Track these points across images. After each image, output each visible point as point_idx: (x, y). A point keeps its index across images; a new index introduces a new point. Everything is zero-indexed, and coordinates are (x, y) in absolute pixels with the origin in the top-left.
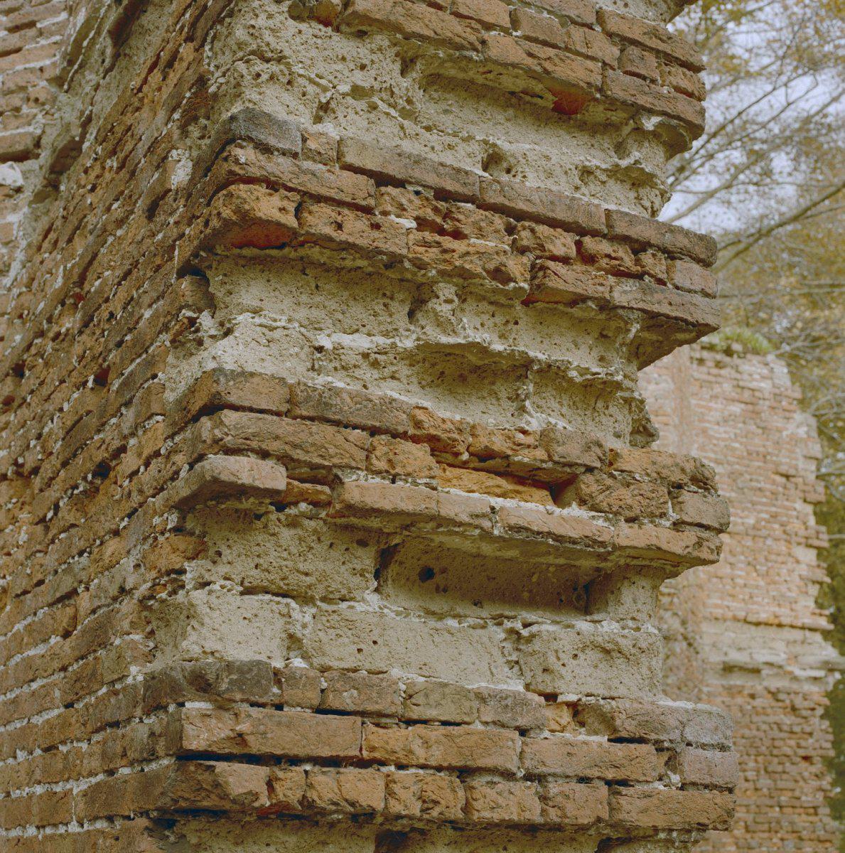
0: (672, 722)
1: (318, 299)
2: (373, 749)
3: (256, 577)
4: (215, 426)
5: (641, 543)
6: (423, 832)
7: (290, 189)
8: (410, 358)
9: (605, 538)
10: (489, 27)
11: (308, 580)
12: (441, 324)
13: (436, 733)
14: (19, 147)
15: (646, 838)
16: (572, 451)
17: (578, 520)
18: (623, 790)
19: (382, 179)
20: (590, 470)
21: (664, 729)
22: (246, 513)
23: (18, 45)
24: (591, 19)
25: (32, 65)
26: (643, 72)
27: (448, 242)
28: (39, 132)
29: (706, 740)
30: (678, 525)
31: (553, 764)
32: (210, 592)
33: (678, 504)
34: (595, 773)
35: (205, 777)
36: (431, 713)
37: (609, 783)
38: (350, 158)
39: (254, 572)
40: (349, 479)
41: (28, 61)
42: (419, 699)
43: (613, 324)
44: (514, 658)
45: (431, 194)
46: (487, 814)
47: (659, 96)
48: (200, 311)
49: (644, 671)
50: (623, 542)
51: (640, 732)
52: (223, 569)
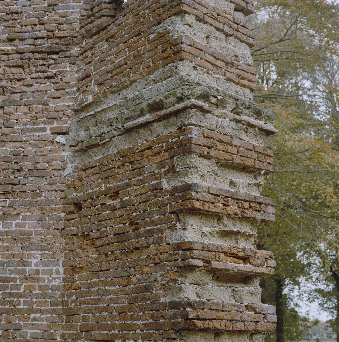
0: (266, 309)
1: (202, 221)
2: (217, 317)
3: (192, 281)
4: (190, 253)
5: (260, 272)
6: (222, 332)
7: (201, 200)
8: (218, 232)
9: (254, 271)
10: (233, 154)
11: (201, 281)
12: (225, 226)
13: (227, 313)
14: (64, 131)
15: (260, 333)
16: (249, 253)
17: (249, 267)
18: (257, 323)
19: (216, 195)
20: (252, 256)
21: (264, 311)
22: (192, 269)
23: (60, 96)
24: (252, 148)
25: (65, 104)
26: (262, 160)
27: (227, 208)
28: (69, 126)
29: (271, 313)
30: (267, 267)
31: (246, 319)
32: (185, 285)
33: (267, 263)
34: (253, 320)
35: (191, 323)
36: (227, 309)
37: (255, 322)
38: (211, 192)
39: (192, 281)
40: (213, 262)
41: (64, 102)
42: (225, 307)
43: (254, 222)
44: (233, 295)
45: (224, 197)
46: (236, 329)
47: (265, 166)
48: (177, 222)
49: (258, 298)
50: (257, 272)
51: (260, 312)
52: (187, 280)
